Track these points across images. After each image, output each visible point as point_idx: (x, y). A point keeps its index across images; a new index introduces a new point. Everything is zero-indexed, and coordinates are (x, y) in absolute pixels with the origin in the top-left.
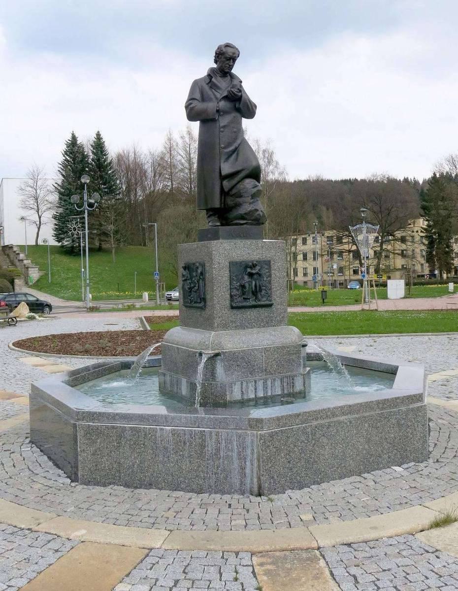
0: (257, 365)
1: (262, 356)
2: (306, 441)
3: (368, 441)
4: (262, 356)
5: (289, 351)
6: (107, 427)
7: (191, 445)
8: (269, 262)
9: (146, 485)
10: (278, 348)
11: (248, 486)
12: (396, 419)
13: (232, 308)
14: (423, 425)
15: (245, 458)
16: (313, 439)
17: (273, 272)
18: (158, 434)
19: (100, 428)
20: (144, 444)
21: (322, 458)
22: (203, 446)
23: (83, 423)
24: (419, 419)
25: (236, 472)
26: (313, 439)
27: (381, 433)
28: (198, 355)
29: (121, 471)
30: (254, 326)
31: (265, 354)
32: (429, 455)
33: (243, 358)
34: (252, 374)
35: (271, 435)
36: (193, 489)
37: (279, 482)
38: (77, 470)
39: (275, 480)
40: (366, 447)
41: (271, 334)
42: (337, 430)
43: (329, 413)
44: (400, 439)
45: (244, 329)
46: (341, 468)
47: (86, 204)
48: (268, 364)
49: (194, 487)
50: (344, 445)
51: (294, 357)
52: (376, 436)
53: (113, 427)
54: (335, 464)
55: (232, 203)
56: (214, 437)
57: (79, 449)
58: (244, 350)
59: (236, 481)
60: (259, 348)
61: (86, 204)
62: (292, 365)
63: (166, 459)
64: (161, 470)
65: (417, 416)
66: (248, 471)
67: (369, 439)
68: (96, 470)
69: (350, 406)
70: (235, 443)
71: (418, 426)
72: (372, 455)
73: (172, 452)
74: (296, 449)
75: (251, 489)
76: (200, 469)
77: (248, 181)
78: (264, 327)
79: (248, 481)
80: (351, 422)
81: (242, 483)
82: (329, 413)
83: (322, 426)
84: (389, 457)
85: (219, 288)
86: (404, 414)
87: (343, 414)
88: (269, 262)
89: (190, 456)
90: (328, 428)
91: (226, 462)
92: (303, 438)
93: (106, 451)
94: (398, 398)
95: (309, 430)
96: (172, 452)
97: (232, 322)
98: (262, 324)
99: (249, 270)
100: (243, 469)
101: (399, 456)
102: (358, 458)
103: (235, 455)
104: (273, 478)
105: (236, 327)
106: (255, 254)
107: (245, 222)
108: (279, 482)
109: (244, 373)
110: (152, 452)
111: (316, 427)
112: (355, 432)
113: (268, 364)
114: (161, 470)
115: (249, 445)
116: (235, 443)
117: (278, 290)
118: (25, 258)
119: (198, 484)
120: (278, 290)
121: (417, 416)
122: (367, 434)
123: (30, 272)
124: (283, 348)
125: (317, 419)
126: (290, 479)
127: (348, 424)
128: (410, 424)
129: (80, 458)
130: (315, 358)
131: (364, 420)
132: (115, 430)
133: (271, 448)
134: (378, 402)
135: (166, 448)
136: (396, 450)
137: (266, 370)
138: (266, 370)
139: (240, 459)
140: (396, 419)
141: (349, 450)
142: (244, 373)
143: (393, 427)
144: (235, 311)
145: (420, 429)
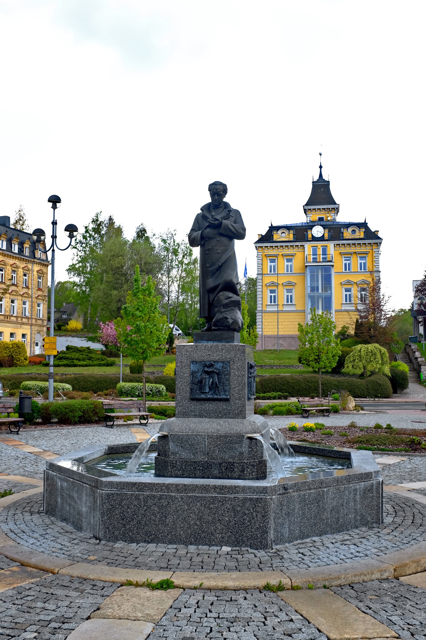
1: (205, 442)
2: (139, 506)
3: (200, 519)
5: (231, 440)
12: (231, 504)
13: (192, 399)
14: (263, 516)
16: (145, 506)
23: (248, 497)
24: (259, 509)
26: (145, 506)
27: (215, 514)
30: (212, 416)
31: (207, 440)
32: (300, 233)
33: (187, 441)
35: (108, 495)
37: (113, 533)
39: (110, 530)
40: (198, 523)
41: (219, 424)
42: (169, 503)
43: (164, 488)
44: (236, 524)
45: (203, 418)
50: (175, 516)
52: (209, 516)
54: (166, 531)
60: (202, 435)
62: (234, 452)
65: (255, 506)
69: (185, 485)
71: (256, 516)
72: (203, 531)
74: (129, 510)
77: (221, 293)
78: (222, 418)
80: (182, 498)
82: (164, 488)
83: (154, 496)
84: (223, 538)
85: (181, 383)
86: (241, 502)
90: (159, 499)
94: (238, 486)
95: (142, 497)
97: (191, 411)
98: (220, 415)
99: (206, 369)
101: (233, 539)
104: (108, 528)
105: (195, 415)
106: (215, 355)
107: (217, 328)
111: (148, 496)
112: (186, 507)
117: (237, 387)
118: (419, 356)
120: (237, 387)
122: (199, 512)
123: (422, 370)
124: (226, 437)
126: (123, 533)
127: (180, 499)
128: (247, 512)
130: (344, 457)
133: (107, 505)
136: (231, 532)
137: (208, 454)
138: (208, 454)
143: (228, 512)
144: (194, 402)
145: (259, 519)
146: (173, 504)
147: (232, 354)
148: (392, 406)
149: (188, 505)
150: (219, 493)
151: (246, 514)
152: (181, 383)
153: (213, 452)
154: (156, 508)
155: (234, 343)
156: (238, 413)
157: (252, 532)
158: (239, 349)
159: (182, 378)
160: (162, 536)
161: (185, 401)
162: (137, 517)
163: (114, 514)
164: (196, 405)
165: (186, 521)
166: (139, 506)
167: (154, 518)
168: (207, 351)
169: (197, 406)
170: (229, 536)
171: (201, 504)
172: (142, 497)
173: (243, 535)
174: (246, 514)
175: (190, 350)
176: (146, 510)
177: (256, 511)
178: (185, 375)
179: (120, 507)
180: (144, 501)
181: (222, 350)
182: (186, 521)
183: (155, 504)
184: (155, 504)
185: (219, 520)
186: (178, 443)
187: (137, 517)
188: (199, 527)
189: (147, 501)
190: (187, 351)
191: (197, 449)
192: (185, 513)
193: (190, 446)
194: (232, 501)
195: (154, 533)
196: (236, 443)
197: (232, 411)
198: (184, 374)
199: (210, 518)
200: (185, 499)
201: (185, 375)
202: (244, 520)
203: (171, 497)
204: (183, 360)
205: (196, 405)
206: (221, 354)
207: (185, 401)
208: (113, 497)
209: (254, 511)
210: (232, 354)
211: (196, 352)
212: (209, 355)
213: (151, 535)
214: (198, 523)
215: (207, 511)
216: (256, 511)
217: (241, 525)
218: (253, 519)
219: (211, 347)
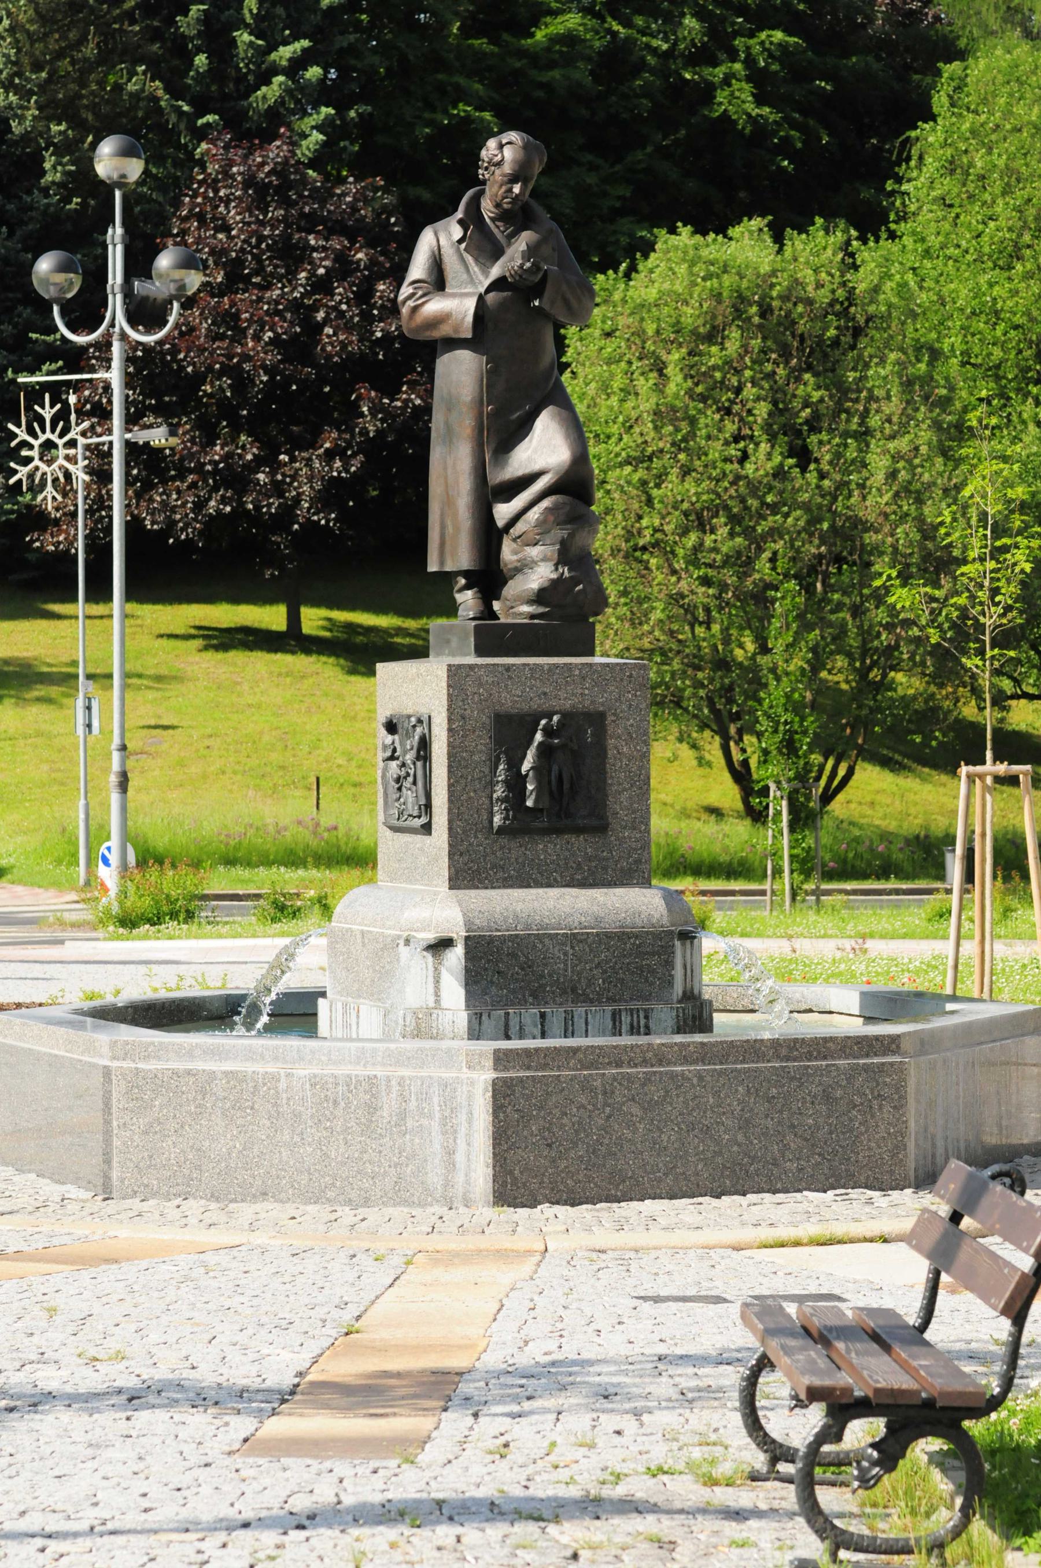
0: (550, 975)
2: (590, 1107)
3: (745, 1125)
4: (565, 954)
5: (639, 946)
6: (175, 1073)
7: (348, 1104)
8: (602, 716)
9: (254, 1196)
10: (608, 936)
11: (461, 1189)
12: (820, 1084)
14: (895, 1108)
15: (455, 1132)
16: (606, 1104)
17: (611, 742)
18: (282, 1085)
19: (160, 1076)
20: (252, 1108)
21: (626, 1146)
22: (372, 1109)
25: (437, 1161)
26: (606, 1104)
27: (781, 1112)
28: (402, 942)
29: (204, 1168)
30: (555, 880)
31: (572, 947)
33: (513, 955)
34: (535, 997)
36: (350, 1200)
37: (524, 1184)
38: (110, 1168)
40: (740, 1137)
42: (667, 1092)
44: (831, 1133)
46: (676, 1179)
47: (116, 306)
48: (579, 974)
49: (353, 1195)
51: (654, 961)
53: (189, 1072)
55: (515, 558)
56: (395, 1088)
57: (115, 1124)
58: (517, 936)
59: (435, 1178)
61: (116, 306)
62: (646, 980)
63: (297, 1139)
64: (287, 1163)
65: (878, 1084)
66: (460, 1157)
67: (747, 1121)
68: (149, 1167)
70: (436, 1100)
73: (310, 1123)
74: (565, 1120)
75: (464, 1194)
76: (366, 1157)
79: (460, 1178)
80: (701, 1078)
81: (447, 1184)
83: (629, 1078)
84: (800, 1170)
85: (463, 781)
87: (686, 1060)
88: (602, 716)
89: (346, 1130)
90: (643, 1085)
91: (417, 1141)
92: (583, 1099)
93: (173, 1125)
95: (598, 1083)
96: (310, 1123)
100: (450, 1153)
101: (826, 1171)
102: (719, 1160)
103: (435, 1126)
105: (505, 879)
106: (562, 694)
108: (524, 1184)
109: (514, 992)
110: (268, 1123)
112: (711, 1100)
113: (579, 974)
114: (287, 1163)
115: (465, 1103)
116: (436, 1100)
119: (360, 1189)
120: (625, 790)
121: (878, 1084)
125: (619, 1064)
127: (695, 1081)
128: (857, 1100)
129: (116, 1142)
131: (735, 1078)
132: (192, 1079)
134: (775, 1044)
135: (297, 1116)
136: (819, 1155)
139: (444, 1133)
140: (820, 1084)
141: (696, 1141)
142: (514, 992)
143: (813, 1103)
145: (886, 1116)
146: (678, 1096)
147: (611, 693)
148: (22, 928)
149: (716, 1094)
150: (788, 1059)
151: (855, 1106)
152: (463, 781)
153: (590, 983)
154: (636, 1110)
155: (591, 653)
156: (630, 869)
157: (870, 1149)
158: (631, 676)
159: (466, 767)
160: (650, 1180)
161: (476, 837)
162: (587, 1136)
163: (525, 1133)
164: (510, 849)
165: (711, 1137)
166: (590, 1107)
167: (630, 1136)
168: (538, 683)
169: (516, 850)
170: (818, 1164)
171: (748, 1090)
172: (598, 1083)
173: (849, 1159)
174: (855, 1106)
175: (490, 680)
176: (609, 1117)
177: (879, 1095)
178: (476, 758)
179: (542, 1113)
180: (605, 1093)
181: (584, 678)
182: (711, 1137)
183: (633, 1100)
184: (633, 1100)
185: (793, 1126)
186: (489, 961)
187: (587, 1136)
188: (744, 1147)
189: (613, 1092)
190: (481, 685)
191: (542, 976)
192: (709, 1114)
193: (523, 969)
194: (822, 1075)
195: (630, 1174)
196: (653, 954)
197: (611, 863)
198: (472, 753)
199: (769, 1123)
200: (709, 1078)
201: (476, 758)
202: (851, 1120)
203: (673, 1076)
204: (469, 711)
205: (510, 849)
206: (579, 691)
207: (476, 837)
208: (524, 1088)
209: (874, 1098)
210: (611, 693)
211: (506, 686)
212: (545, 694)
213: (624, 1181)
214: (740, 1137)
215: (762, 1107)
216: (879, 1095)
217: (843, 1133)
218: (873, 1116)
219: (550, 670)
